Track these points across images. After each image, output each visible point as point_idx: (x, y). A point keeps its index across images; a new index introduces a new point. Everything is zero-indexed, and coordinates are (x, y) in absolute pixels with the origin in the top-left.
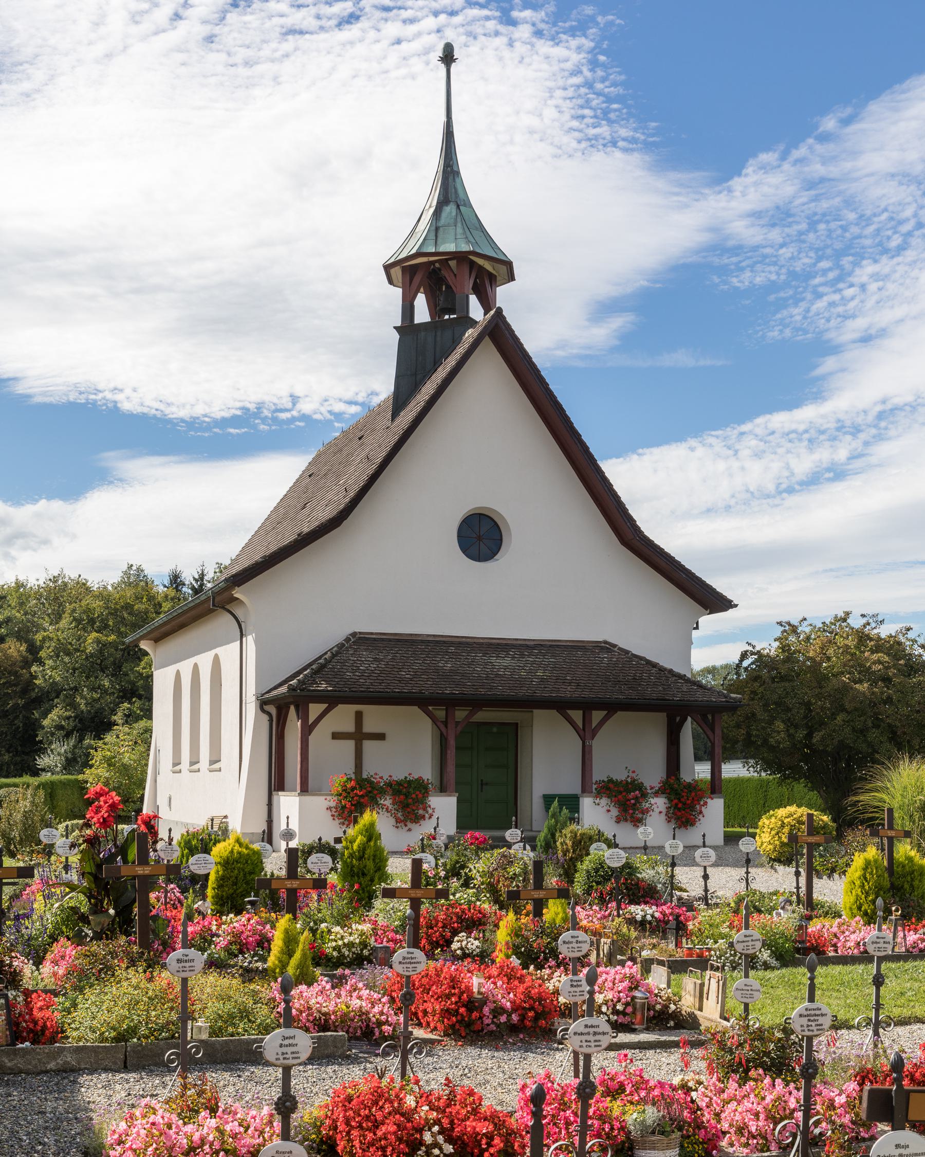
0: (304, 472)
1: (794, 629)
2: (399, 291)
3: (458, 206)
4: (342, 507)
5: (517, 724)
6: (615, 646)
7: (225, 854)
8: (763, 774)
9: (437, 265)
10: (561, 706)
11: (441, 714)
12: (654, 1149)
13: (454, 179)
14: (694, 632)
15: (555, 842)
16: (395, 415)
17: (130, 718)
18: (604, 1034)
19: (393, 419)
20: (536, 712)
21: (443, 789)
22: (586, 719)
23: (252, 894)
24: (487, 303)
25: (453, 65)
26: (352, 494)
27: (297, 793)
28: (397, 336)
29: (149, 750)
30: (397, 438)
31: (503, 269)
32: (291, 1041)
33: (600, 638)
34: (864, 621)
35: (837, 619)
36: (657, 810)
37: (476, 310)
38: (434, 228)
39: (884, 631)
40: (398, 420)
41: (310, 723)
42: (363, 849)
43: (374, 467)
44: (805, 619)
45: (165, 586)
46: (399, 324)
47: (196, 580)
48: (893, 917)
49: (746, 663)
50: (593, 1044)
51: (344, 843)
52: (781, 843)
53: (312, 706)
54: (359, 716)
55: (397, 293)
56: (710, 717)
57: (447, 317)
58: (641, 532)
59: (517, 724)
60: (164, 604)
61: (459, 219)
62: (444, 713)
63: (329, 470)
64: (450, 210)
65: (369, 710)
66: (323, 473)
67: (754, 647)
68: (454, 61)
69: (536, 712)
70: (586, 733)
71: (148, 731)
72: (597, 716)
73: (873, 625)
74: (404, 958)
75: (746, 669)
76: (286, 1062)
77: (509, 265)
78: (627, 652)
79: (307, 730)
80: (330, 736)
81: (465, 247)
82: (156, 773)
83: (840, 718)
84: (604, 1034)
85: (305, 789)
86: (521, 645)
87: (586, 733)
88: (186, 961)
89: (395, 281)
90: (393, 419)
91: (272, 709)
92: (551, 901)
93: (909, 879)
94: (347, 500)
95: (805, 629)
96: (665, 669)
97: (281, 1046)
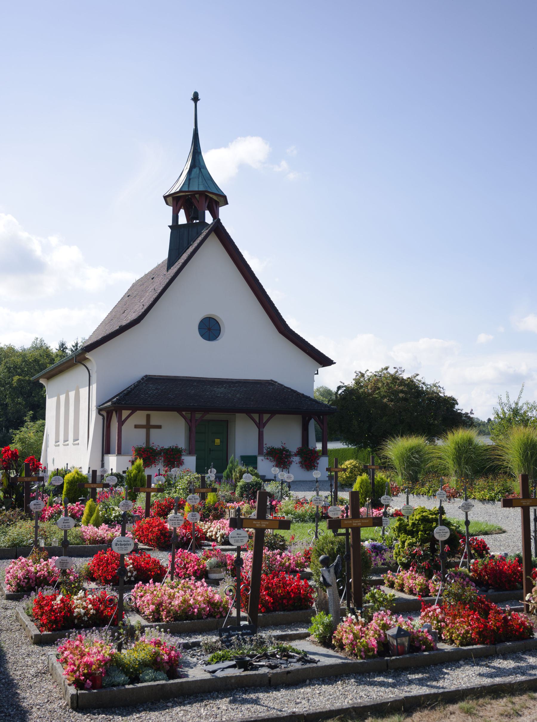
0: (126, 294)
1: (363, 375)
2: (171, 208)
3: (200, 169)
4: (140, 314)
5: (228, 421)
6: (276, 382)
7: (71, 479)
8: (350, 446)
9: (189, 196)
10: (248, 412)
11: (189, 416)
12: (215, 573)
13: (198, 156)
14: (315, 376)
15: (232, 474)
16: (169, 268)
17: (34, 419)
18: (181, 520)
19: (167, 271)
20: (237, 414)
21: (190, 453)
22: (261, 419)
23: (82, 496)
24: (215, 215)
25: (198, 102)
26: (145, 307)
27: (115, 455)
28: (169, 230)
29: (43, 435)
30: (168, 280)
31: (222, 199)
32: (67, 521)
33: (268, 378)
34: (396, 370)
35: (383, 370)
36: (295, 462)
37: (209, 219)
38: (188, 179)
39: (405, 376)
40: (170, 271)
41: (123, 420)
42: (136, 476)
43: (157, 294)
44: (368, 370)
45: (57, 350)
46: (171, 224)
47: (74, 346)
48: (367, 503)
49: (340, 392)
50: (177, 524)
51: (127, 474)
52: (346, 476)
53: (123, 411)
54: (148, 417)
55: (170, 209)
56: (321, 417)
57: (195, 221)
58: (289, 327)
59: (228, 421)
60: (56, 359)
61: (200, 175)
62: (190, 415)
63: (137, 294)
64: (196, 171)
65: (153, 413)
66: (134, 295)
67: (343, 384)
68: (199, 100)
69: (238, 415)
70: (261, 425)
71: (43, 425)
72: (266, 417)
73: (400, 373)
74: (124, 504)
75: (340, 394)
76: (65, 528)
77: (225, 197)
78: (282, 385)
79: (121, 423)
80: (134, 427)
81: (202, 188)
82: (47, 446)
83: (384, 419)
84: (181, 520)
85: (119, 453)
86: (230, 382)
87: (261, 425)
88: (37, 505)
89: (169, 203)
90: (167, 271)
91: (105, 413)
92: (209, 494)
93: (381, 487)
94: (143, 310)
95: (369, 374)
96: (300, 394)
97: (64, 523)
